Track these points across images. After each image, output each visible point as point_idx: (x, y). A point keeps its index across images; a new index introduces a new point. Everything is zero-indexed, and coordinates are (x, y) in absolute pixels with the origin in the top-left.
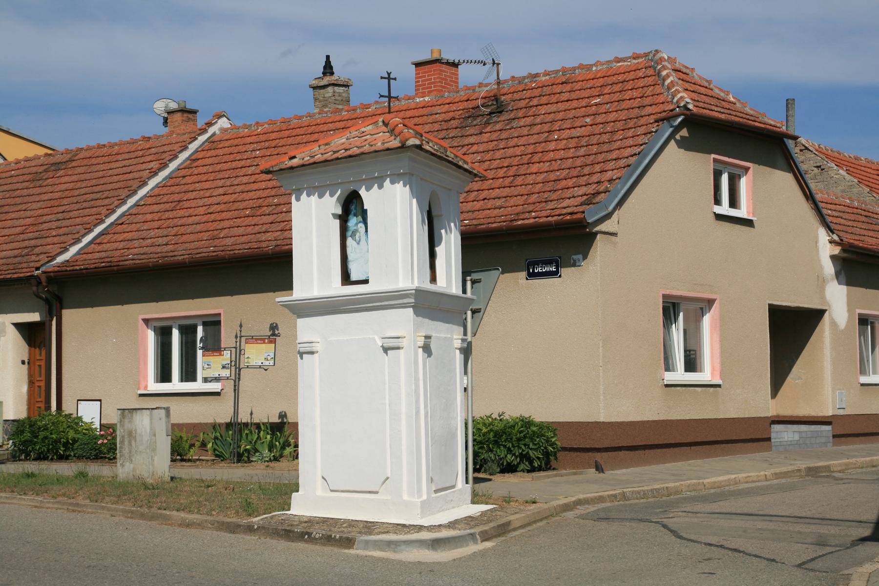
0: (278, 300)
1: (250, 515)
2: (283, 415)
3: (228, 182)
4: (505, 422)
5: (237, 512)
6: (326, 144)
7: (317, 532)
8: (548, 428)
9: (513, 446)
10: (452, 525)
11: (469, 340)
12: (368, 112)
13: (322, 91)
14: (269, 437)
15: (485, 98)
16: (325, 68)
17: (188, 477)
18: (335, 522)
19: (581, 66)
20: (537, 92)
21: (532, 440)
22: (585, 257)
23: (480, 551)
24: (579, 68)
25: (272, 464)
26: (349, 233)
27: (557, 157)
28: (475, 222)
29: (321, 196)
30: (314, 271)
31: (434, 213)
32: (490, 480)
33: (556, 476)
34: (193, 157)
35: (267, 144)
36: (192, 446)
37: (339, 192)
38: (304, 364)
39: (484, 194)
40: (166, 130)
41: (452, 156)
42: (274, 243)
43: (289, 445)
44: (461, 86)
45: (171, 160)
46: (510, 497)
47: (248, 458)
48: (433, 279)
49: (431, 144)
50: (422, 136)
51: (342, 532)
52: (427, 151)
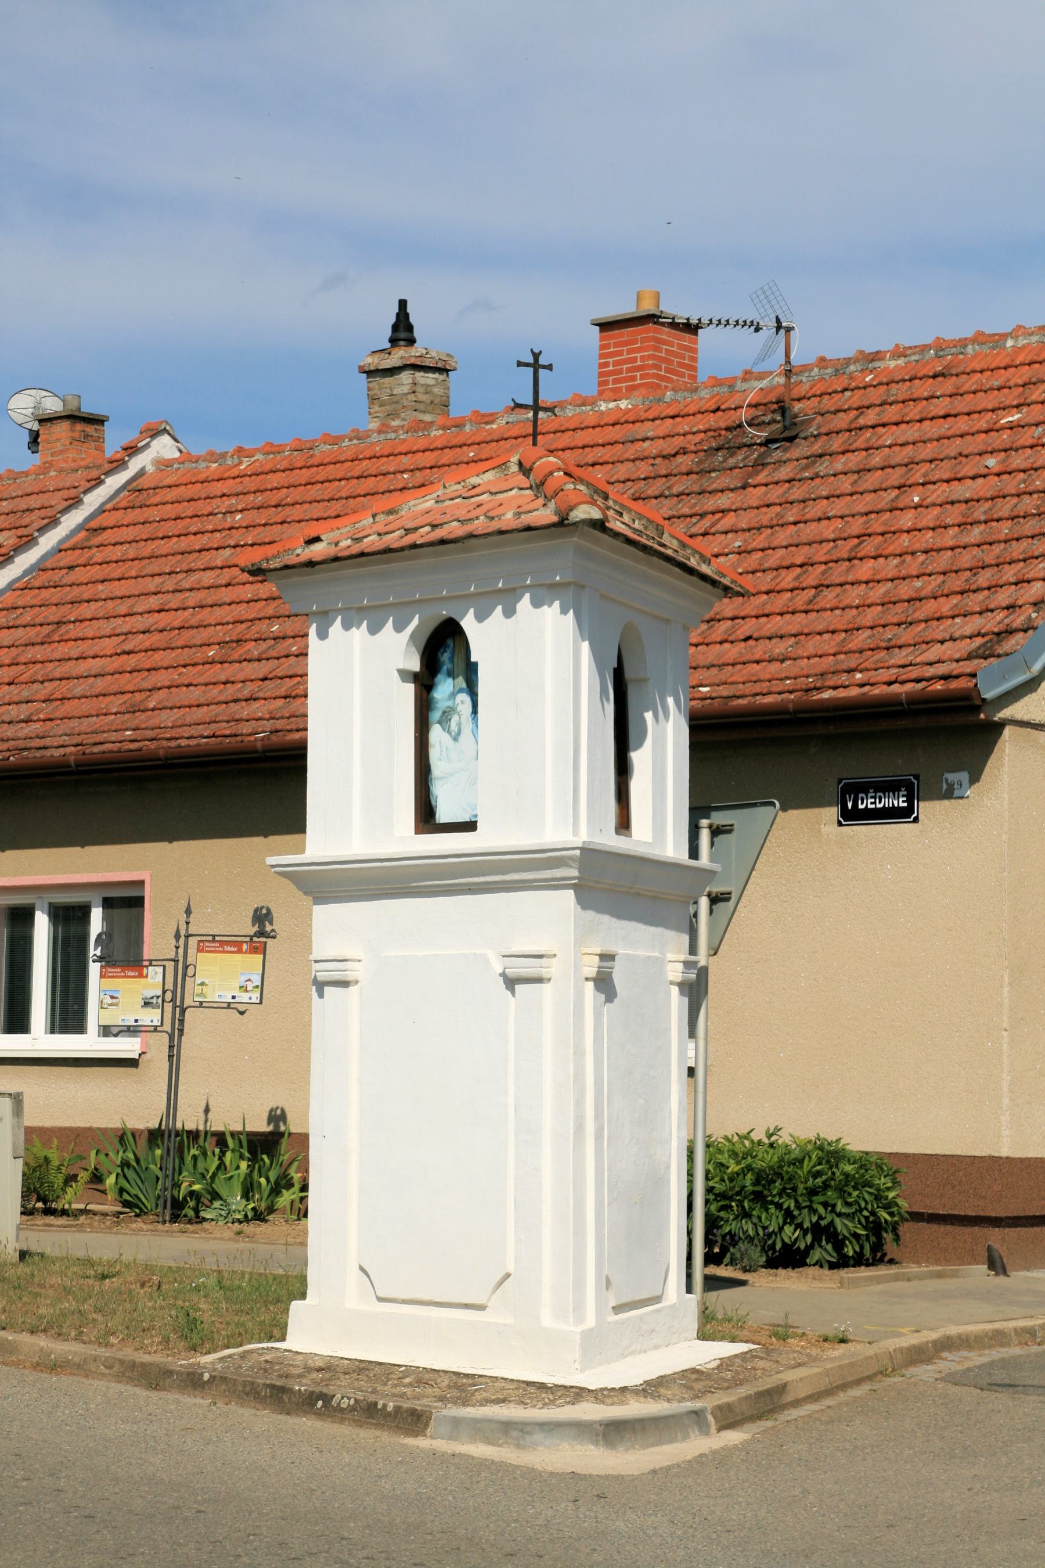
0: (271, 860)
1: (194, 1348)
2: (277, 1117)
3: (170, 583)
4: (781, 1151)
5: (166, 1341)
6: (390, 512)
7: (344, 1394)
8: (879, 1167)
9: (799, 1207)
10: (651, 1388)
11: (702, 963)
12: (490, 432)
13: (387, 380)
14: (244, 1165)
15: (756, 406)
16: (395, 328)
17: (58, 1253)
18: (385, 1371)
19: (980, 338)
20: (875, 396)
21: (842, 1192)
22: (975, 778)
23: (714, 1453)
24: (974, 340)
25: (249, 1228)
26: (435, 716)
27: (917, 546)
28: (724, 691)
29: (374, 630)
30: (354, 794)
31: (629, 674)
32: (742, 1283)
33: (896, 1278)
34: (94, 524)
35: (260, 499)
36: (71, 1178)
37: (415, 622)
38: (327, 1009)
39: (748, 627)
40: (34, 460)
41: (675, 544)
42: (269, 725)
43: (290, 1185)
44: (702, 377)
45: (42, 530)
46: (788, 1326)
47: (197, 1211)
48: (624, 824)
49: (626, 518)
50: (606, 497)
51: (402, 1395)
52: (616, 535)
